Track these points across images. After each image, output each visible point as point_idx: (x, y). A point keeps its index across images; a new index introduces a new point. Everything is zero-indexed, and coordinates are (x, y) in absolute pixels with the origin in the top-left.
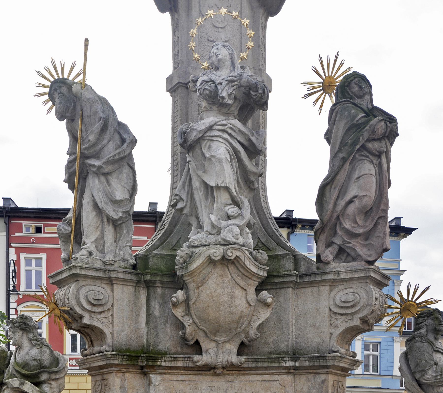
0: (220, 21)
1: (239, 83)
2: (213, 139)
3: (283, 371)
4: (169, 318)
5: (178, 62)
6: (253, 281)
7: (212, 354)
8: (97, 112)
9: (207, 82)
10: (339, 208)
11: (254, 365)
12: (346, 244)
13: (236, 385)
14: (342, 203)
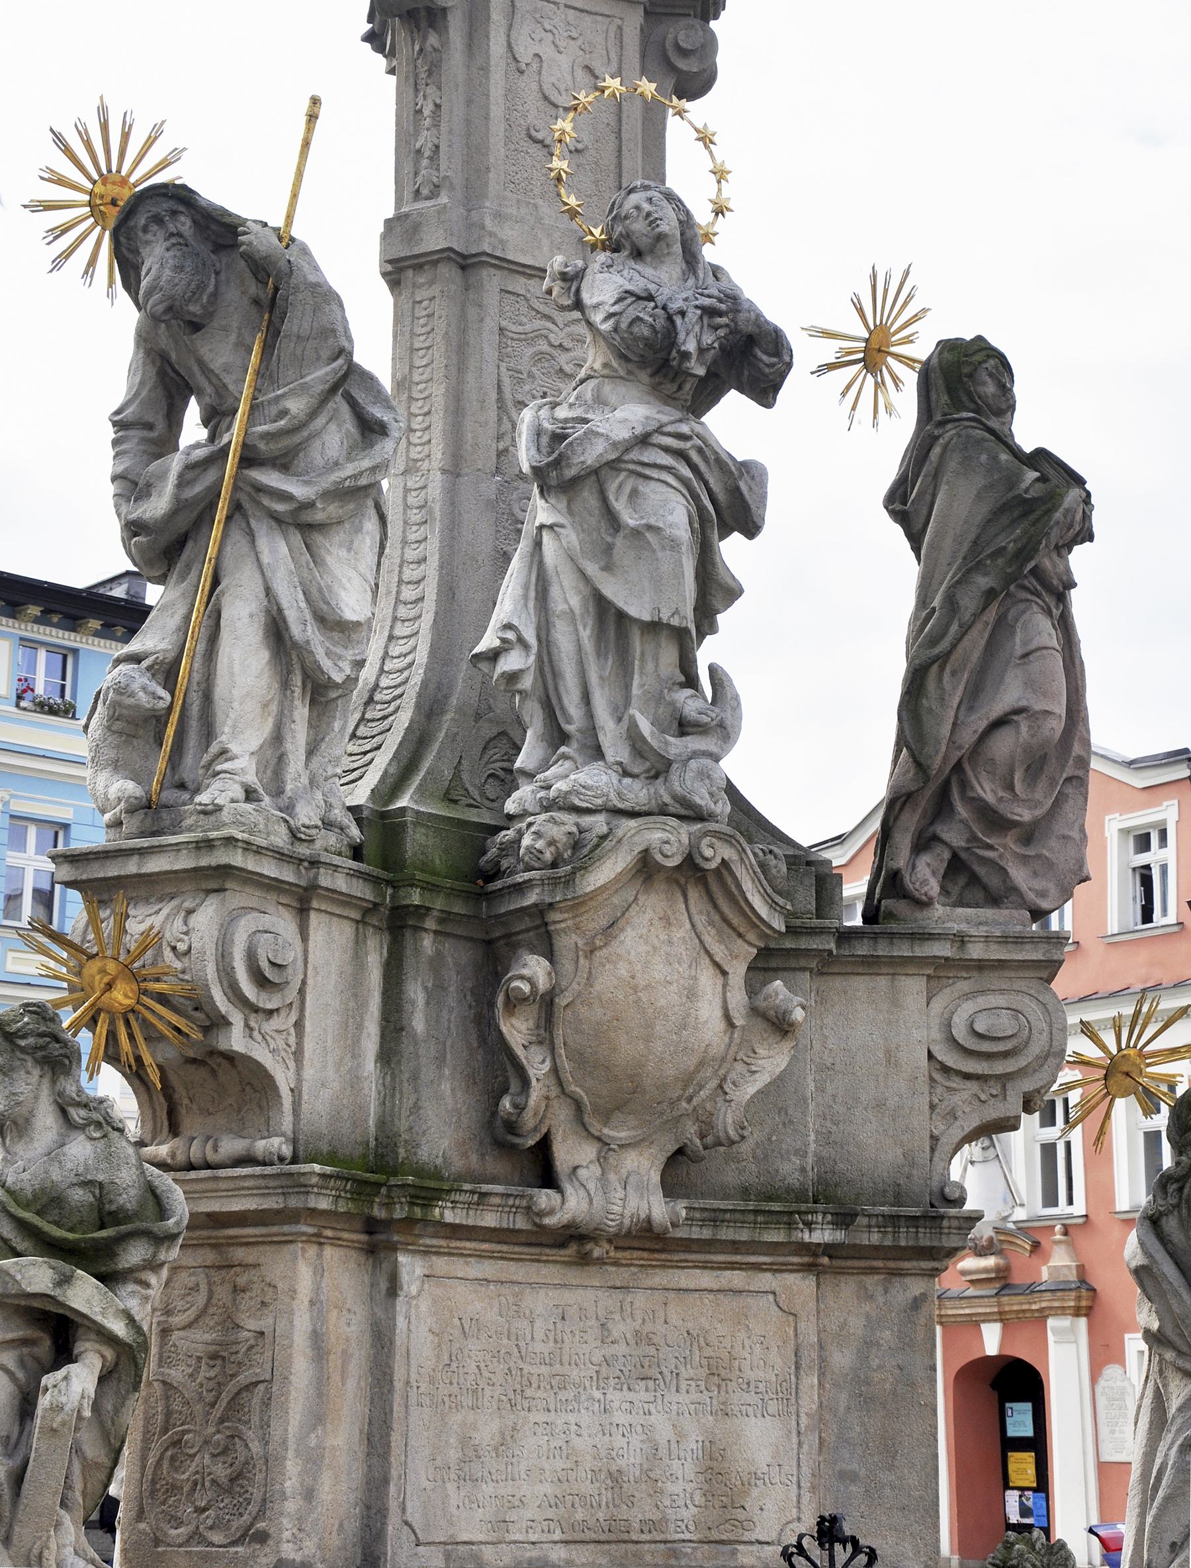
0: (562, 87)
1: (732, 320)
2: (648, 472)
3: (796, 1260)
4: (448, 1043)
5: (435, 180)
6: (746, 946)
7: (591, 1186)
8: (334, 331)
9: (639, 298)
10: (968, 737)
11: (706, 1234)
12: (978, 851)
13: (637, 1304)
14: (978, 722)
